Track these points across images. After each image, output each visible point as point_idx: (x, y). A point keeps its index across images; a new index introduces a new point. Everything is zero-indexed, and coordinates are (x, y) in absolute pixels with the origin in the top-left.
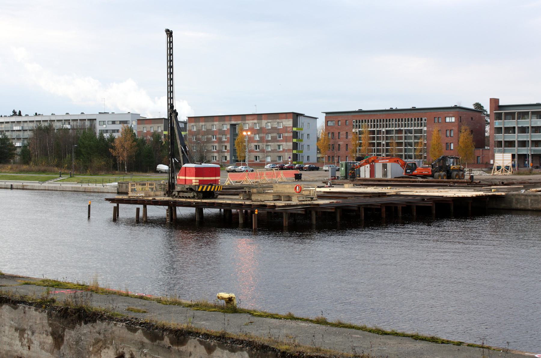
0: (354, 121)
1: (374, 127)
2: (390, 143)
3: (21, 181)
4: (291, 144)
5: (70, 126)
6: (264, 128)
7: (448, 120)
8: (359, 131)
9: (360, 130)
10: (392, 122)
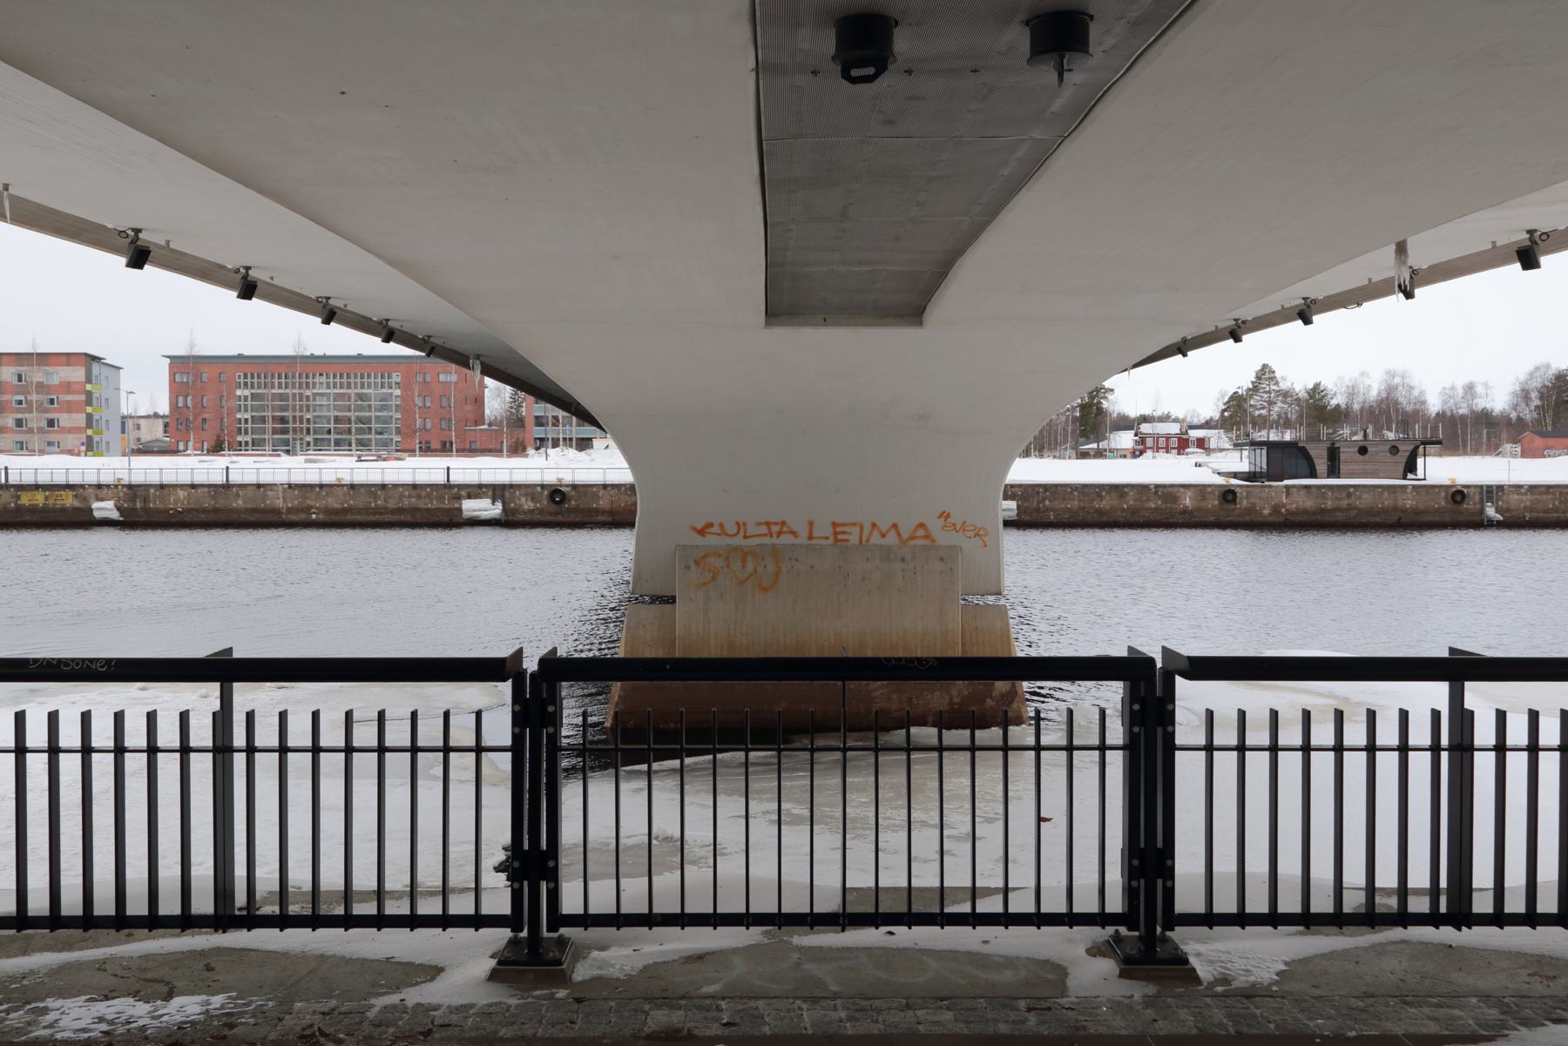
0: (240, 376)
1: (286, 387)
2: (1326, 475)
3: (1179, 967)
4: (84, 415)
5: (88, 411)
6: (6, 382)
7: (442, 377)
8: (252, 394)
9: (253, 391)
10: (313, 378)
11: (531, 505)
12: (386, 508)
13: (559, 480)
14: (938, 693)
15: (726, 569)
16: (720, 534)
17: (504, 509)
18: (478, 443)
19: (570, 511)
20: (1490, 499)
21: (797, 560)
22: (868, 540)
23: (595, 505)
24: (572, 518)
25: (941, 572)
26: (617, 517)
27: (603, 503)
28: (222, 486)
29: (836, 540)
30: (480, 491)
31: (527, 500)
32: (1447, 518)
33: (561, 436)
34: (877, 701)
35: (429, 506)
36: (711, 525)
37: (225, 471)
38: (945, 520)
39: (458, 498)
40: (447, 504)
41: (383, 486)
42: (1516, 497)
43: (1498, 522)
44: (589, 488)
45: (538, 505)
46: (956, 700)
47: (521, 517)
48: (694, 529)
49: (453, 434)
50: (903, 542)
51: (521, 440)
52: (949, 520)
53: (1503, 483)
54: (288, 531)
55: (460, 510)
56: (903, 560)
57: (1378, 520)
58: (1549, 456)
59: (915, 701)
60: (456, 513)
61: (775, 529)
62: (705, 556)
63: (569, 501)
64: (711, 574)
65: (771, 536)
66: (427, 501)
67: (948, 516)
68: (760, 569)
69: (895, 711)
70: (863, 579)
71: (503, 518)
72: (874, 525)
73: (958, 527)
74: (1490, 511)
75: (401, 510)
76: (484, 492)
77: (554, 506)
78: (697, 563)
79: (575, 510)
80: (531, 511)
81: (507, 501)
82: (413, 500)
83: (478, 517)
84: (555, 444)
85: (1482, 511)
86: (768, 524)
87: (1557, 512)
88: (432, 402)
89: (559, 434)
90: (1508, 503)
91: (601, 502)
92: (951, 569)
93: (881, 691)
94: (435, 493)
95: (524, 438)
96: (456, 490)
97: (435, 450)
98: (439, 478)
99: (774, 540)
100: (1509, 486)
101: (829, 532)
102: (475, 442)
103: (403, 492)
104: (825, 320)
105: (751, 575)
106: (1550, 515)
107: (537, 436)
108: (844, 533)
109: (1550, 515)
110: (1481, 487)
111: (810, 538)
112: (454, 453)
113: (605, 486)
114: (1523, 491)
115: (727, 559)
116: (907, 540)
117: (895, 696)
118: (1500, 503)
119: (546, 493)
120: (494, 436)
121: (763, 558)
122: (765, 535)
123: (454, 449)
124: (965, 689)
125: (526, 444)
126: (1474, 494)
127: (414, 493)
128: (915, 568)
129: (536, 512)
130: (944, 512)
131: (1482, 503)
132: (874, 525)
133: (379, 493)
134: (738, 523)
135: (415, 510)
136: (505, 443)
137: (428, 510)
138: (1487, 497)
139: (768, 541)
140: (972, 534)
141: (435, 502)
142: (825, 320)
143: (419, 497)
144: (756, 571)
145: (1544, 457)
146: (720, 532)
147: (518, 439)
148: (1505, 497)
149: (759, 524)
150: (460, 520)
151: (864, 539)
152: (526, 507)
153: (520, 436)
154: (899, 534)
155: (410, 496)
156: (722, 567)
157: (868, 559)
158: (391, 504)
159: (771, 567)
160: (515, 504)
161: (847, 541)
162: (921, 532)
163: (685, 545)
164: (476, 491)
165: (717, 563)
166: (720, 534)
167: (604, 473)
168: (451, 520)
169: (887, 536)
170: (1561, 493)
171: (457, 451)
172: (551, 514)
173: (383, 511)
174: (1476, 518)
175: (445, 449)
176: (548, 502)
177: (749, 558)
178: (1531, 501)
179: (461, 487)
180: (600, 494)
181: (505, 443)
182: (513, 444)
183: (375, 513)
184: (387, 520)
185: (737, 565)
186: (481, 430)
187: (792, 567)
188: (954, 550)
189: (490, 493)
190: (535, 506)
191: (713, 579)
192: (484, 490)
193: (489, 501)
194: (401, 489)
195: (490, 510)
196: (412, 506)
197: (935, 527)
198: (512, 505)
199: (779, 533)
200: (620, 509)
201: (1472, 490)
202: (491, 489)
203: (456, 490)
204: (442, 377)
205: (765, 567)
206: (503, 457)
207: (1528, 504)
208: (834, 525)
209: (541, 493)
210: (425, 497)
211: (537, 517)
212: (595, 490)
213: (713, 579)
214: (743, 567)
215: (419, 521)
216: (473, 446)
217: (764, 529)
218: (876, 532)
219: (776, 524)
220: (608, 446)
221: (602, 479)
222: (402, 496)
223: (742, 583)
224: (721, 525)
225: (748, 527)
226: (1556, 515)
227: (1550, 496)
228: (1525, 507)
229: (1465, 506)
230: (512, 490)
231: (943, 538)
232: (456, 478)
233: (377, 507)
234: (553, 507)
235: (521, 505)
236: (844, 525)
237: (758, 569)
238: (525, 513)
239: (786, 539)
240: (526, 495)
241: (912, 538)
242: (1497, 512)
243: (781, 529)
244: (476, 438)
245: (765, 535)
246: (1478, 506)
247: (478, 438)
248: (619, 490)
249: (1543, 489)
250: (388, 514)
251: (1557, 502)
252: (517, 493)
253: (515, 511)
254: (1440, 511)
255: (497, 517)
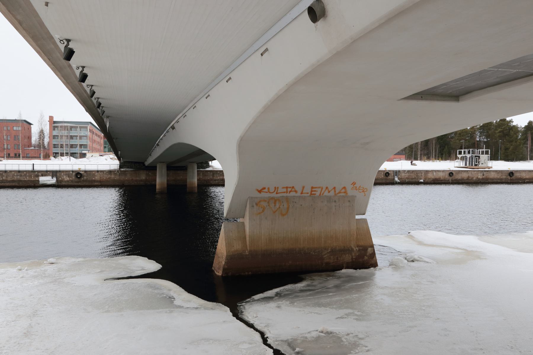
7: (15, 128)
11: (68, 179)
12: (7, 180)
13: (80, 169)
14: (347, 255)
15: (268, 207)
16: (267, 192)
17: (57, 181)
18: (30, 154)
19: (84, 181)
20: (396, 175)
21: (296, 203)
22: (323, 194)
23: (94, 179)
24: (84, 184)
25: (349, 206)
26: (102, 183)
27: (97, 178)
28: (32, 171)
29: (311, 194)
30: (47, 173)
31: (66, 177)
32: (384, 181)
33: (65, 152)
34: (325, 259)
35: (26, 179)
36: (264, 188)
37: (32, 165)
38: (353, 186)
39: (38, 176)
40: (33, 179)
41: (6, 172)
42: (404, 174)
43: (398, 182)
44: (91, 172)
45: (71, 179)
46: (354, 257)
47: (63, 183)
48: (257, 190)
49: (21, 150)
50: (336, 195)
51: (48, 153)
52: (355, 185)
53: (400, 170)
54: (19, 190)
55: (38, 181)
56: (335, 202)
57: (126, 178)
58: (395, 161)
59: (339, 258)
60: (37, 182)
61: (289, 190)
62: (260, 202)
63: (84, 177)
64: (262, 209)
65: (287, 193)
66: (24, 177)
67: (355, 184)
68: (281, 207)
69: (332, 263)
70: (321, 209)
71: (57, 184)
72: (327, 188)
73: (357, 188)
74: (396, 179)
75: (13, 181)
76: (48, 174)
77: (77, 179)
78: (257, 204)
79: (86, 181)
80: (68, 181)
81: (58, 177)
82: (19, 177)
83: (46, 183)
84: (62, 155)
85: (394, 179)
86: (287, 188)
87: (415, 179)
88: (10, 138)
89: (64, 151)
90: (401, 176)
91: (96, 178)
92: (352, 205)
93: (327, 255)
94: (28, 174)
95: (49, 152)
96: (37, 173)
97: (12, 157)
98: (30, 168)
99: (288, 195)
100: (402, 171)
101: (309, 191)
102: (29, 154)
103: (14, 174)
104: (422, 97)
105: (278, 209)
106: (413, 180)
107: (54, 152)
108: (315, 191)
109: (413, 180)
110: (394, 171)
111: (302, 193)
112: (21, 158)
113: (98, 171)
114: (406, 172)
115: (268, 202)
116: (338, 193)
117: (332, 257)
118: (399, 176)
119: (74, 174)
120: (36, 152)
121: (282, 202)
122: (284, 192)
123: (21, 157)
124: (357, 253)
125: (50, 154)
126: (392, 173)
127: (19, 174)
128: (339, 205)
129: (70, 181)
130: (354, 182)
131: (394, 176)
132: (327, 188)
133: (4, 174)
134: (275, 188)
135: (20, 181)
136: (42, 154)
137: (25, 181)
138: (396, 174)
139: (285, 195)
140: (362, 191)
141: (28, 178)
142: (422, 97)
143: (21, 176)
144: (280, 207)
145: (394, 161)
146: (267, 191)
147: (47, 153)
148: (401, 174)
149: (283, 188)
150: (38, 185)
151: (322, 194)
152: (66, 179)
153: (48, 152)
154: (335, 191)
155: (17, 175)
156: (267, 206)
157: (322, 202)
158: (9, 179)
159: (286, 206)
160: (61, 178)
161: (315, 194)
162: (343, 191)
163: (252, 197)
164: (45, 173)
165: (264, 204)
166: (267, 192)
167: (98, 166)
168: (34, 185)
169: (330, 193)
170: (416, 173)
171: (22, 157)
172: (76, 182)
173: (5, 181)
174: (392, 181)
175: (17, 156)
176: (75, 177)
177: (277, 202)
178: (408, 175)
179: (39, 172)
180: (96, 174)
181: (42, 154)
182: (45, 155)
183: (2, 182)
184: (7, 185)
185: (272, 205)
186: (31, 149)
187: (294, 206)
188: (354, 197)
189: (51, 174)
190: (69, 179)
191: (263, 211)
192: (48, 173)
193: (51, 177)
194: (13, 173)
195: (51, 181)
196: (18, 179)
197: (349, 188)
198: (60, 179)
199: (290, 191)
200: (104, 180)
201: (391, 172)
202: (51, 173)
203: (37, 173)
204: (15, 128)
205: (283, 205)
206: (20, 159)
207: (407, 176)
208: (312, 188)
209: (72, 174)
210: (24, 176)
211: (70, 184)
212: (94, 173)
213: (263, 211)
214: (275, 206)
215: (21, 185)
216: (28, 156)
217: (285, 190)
218: (327, 190)
219: (290, 187)
220: (92, 156)
221: (18, 169)
222: (14, 175)
223: (274, 212)
224: (269, 188)
225: (279, 189)
226: (415, 180)
227: (413, 174)
228: (406, 177)
229: (389, 177)
230: (60, 173)
231: (350, 192)
232: (37, 168)
233: (3, 180)
234: (77, 180)
235: (63, 179)
236: (316, 188)
237: (281, 207)
238: (65, 182)
239: (293, 194)
240: (66, 175)
241: (340, 193)
242: (398, 179)
243: (292, 190)
244: (29, 153)
245: (284, 192)
246: (393, 177)
247: (30, 152)
248: (103, 173)
249: (411, 172)
250: (7, 182)
251: (415, 176)
252: (62, 174)
253: (61, 181)
254: (382, 179)
255: (54, 183)
